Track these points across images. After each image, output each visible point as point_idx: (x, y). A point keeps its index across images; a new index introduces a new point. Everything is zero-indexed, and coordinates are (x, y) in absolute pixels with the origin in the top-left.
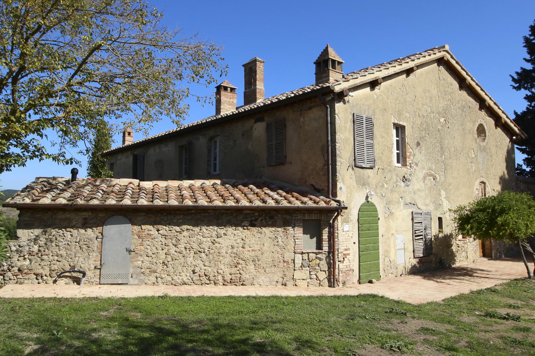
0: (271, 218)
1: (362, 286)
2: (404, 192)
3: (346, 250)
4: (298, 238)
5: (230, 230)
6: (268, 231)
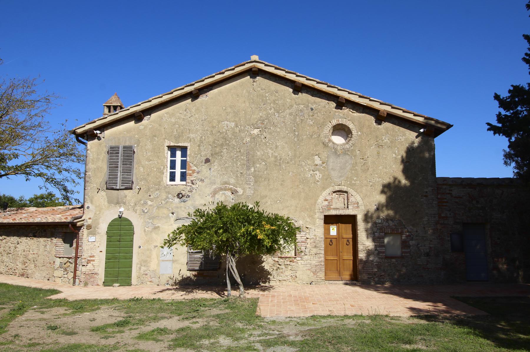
0: (45, 231)
1: (76, 288)
2: (177, 208)
3: (91, 257)
4: (56, 246)
5: (24, 240)
6: (42, 240)
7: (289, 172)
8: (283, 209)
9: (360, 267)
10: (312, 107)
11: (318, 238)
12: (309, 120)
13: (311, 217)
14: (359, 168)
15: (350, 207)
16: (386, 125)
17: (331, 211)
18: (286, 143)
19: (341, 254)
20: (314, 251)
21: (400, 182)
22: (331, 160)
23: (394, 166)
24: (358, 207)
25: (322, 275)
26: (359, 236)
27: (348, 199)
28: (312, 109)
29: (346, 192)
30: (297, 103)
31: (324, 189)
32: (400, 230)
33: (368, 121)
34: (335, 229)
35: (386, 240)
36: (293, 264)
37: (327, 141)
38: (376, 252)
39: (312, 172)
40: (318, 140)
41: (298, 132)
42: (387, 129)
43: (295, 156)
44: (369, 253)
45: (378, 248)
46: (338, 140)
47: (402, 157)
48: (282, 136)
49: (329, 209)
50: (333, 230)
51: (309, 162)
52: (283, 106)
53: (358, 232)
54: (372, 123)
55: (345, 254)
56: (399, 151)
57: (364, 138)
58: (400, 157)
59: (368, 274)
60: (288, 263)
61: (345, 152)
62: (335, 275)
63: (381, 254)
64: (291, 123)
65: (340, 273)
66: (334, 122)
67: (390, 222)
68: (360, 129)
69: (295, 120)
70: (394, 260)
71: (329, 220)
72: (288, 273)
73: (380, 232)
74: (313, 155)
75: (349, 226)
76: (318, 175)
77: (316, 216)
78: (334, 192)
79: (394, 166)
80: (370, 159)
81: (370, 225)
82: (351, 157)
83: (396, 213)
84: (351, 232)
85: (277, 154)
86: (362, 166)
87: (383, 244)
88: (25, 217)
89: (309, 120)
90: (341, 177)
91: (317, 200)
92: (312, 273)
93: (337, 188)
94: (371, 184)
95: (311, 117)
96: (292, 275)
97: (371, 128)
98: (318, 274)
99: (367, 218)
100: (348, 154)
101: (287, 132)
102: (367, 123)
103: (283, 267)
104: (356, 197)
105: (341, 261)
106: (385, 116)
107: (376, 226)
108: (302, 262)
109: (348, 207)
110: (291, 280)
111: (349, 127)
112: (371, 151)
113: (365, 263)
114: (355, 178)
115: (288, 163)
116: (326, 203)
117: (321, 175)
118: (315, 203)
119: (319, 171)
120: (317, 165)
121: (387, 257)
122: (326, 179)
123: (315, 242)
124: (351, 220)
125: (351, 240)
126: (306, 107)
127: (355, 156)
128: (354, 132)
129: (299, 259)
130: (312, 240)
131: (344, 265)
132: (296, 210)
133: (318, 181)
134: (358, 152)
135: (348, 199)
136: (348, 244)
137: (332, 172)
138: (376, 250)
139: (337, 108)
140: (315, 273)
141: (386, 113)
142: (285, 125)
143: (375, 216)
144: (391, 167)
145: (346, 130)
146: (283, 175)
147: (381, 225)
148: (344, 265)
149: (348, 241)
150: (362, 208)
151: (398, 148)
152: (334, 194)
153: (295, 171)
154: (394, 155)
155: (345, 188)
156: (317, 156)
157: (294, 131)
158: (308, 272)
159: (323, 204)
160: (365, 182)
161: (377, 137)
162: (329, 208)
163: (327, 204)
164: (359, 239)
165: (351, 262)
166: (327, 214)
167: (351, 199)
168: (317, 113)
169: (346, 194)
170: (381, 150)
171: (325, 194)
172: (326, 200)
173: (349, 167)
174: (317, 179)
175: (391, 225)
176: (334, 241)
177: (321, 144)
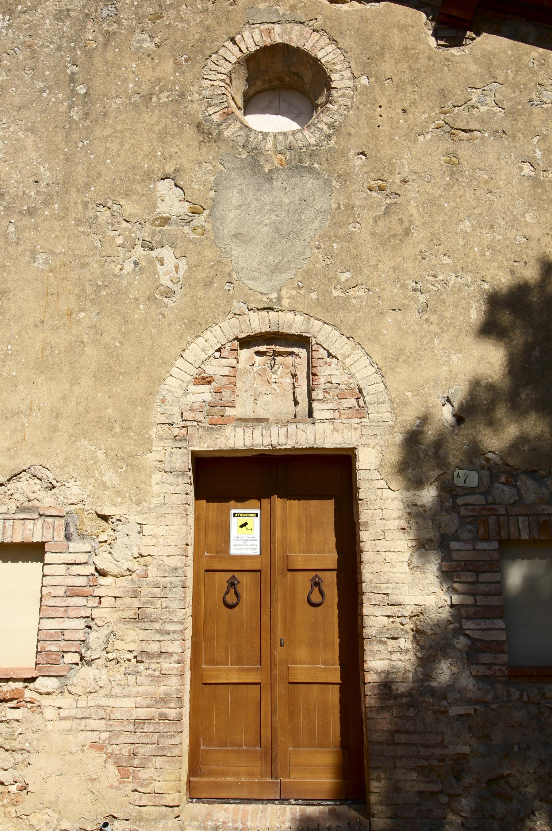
7: (34, 255)
9: (380, 724)
11: (153, 572)
12: (138, 36)
14: (363, 230)
17: (229, 430)
18: (32, 130)
19: (280, 653)
20: (132, 639)
22: (233, 197)
23: (529, 218)
24: (361, 410)
25: (170, 775)
26: (366, 556)
27: (311, 375)
29: (303, 341)
31: (196, 326)
33: (402, 28)
34: (255, 523)
37: (216, 118)
38: (461, 642)
39: (139, 252)
40: (175, 114)
41: (87, 82)
42: (487, 61)
43: (67, 182)
44: (432, 642)
45: (468, 625)
48: (17, 100)
49: (216, 425)
50: (245, 533)
51: (129, 208)
53: (364, 535)
54: (418, 39)
55: (302, 653)
57: (383, 101)
59: (420, 770)
61: (299, 161)
62: (246, 771)
63: (486, 658)
64: (59, 48)
65: (272, 760)
67: (527, 485)
68: (368, 63)
69: (76, 38)
71: (220, 478)
73: (476, 539)
74: (149, 177)
75: (325, 509)
77: (152, 458)
78: (246, 342)
79: (529, 218)
80: (413, 190)
81: (429, 495)
82: (328, 183)
84: (332, 541)
87: (495, 601)
88: (267, 219)
89: (138, 36)
90: (277, 269)
92: (112, 771)
93: (258, 323)
94: (422, 298)
97: (416, 59)
98: (144, 774)
99: (418, 454)
102: (396, 39)
104: (348, 363)
105: (281, 689)
107: (455, 507)
108: (64, 701)
109: (310, 414)
111: (316, 60)
112: (419, 156)
113: (411, 699)
114: (345, 276)
115: (31, 212)
116: (204, 393)
117: (183, 264)
118: (151, 393)
119: (173, 245)
120: (166, 221)
121: (518, 674)
122: (208, 284)
123: (135, 595)
124: (326, 475)
125: (330, 581)
127: (343, 178)
128: (340, 79)
129: (51, 684)
131: (293, 713)
132: (55, 430)
133: (169, 293)
134: (359, 161)
135: (311, 375)
136: (316, 598)
137: (238, 254)
140: (126, 767)
142: (34, 55)
144: (514, 219)
147: (478, 499)
148: (293, 713)
149: (316, 584)
150: (381, 413)
152: (246, 354)
153: (59, 249)
154: (527, 169)
155: (294, 324)
157: (72, 78)
158: (94, 762)
159: (190, 398)
160: (392, 292)
161: (443, 94)
162: (216, 415)
163: (208, 397)
164: (368, 573)
165: (334, 696)
167: (327, 372)
169: (303, 352)
172: (206, 380)
173: (314, 226)
174: (166, 281)
175: (530, 498)
176: (245, 579)
177: (190, 132)
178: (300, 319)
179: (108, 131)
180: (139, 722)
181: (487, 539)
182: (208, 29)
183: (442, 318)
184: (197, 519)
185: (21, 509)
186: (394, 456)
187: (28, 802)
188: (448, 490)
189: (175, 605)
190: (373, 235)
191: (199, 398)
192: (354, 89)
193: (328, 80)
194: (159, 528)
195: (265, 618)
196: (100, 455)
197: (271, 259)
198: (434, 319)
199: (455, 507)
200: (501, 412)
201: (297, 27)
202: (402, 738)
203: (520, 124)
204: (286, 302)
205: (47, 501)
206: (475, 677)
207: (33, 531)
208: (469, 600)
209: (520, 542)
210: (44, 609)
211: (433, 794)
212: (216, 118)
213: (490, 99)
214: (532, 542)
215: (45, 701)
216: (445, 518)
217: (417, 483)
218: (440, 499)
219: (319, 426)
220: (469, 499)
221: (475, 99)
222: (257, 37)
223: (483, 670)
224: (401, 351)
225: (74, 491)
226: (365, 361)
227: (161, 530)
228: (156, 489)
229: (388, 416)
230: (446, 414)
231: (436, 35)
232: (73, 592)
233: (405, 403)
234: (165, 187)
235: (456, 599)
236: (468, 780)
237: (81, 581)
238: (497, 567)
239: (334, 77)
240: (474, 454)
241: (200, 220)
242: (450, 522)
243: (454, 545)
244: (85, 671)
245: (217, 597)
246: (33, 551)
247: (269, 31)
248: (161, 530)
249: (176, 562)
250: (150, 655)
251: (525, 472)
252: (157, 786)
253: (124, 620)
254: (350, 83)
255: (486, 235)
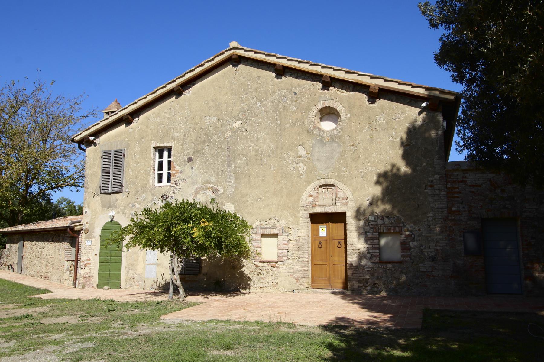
7: (271, 167)
8: (264, 208)
10: (296, 91)
11: (301, 240)
12: (292, 106)
13: (294, 215)
15: (338, 203)
16: (382, 103)
17: (317, 208)
18: (268, 134)
19: (331, 258)
20: (297, 254)
21: (398, 169)
22: (317, 150)
23: (390, 152)
24: (347, 203)
25: (307, 281)
28: (295, 93)
29: (334, 186)
30: (280, 89)
31: (308, 183)
32: (397, 230)
33: (359, 99)
34: (325, 229)
35: (383, 241)
36: (275, 269)
37: (312, 128)
38: (369, 255)
39: (295, 165)
41: (280, 120)
44: (361, 256)
45: (370, 251)
46: (328, 126)
47: (401, 139)
48: (264, 127)
49: (314, 206)
50: (323, 231)
52: (266, 93)
54: (364, 103)
56: (396, 133)
57: (354, 121)
58: (398, 139)
59: (359, 282)
60: (270, 268)
61: (333, 138)
63: (374, 258)
64: (273, 111)
65: (329, 280)
66: (320, 106)
67: (386, 220)
68: (350, 110)
70: (390, 266)
71: (317, 219)
72: (269, 279)
73: (373, 232)
74: (296, 145)
75: (343, 224)
76: (302, 168)
77: (300, 215)
78: (320, 186)
79: (390, 152)
80: (361, 145)
81: (362, 223)
83: (394, 207)
85: (258, 148)
86: (352, 154)
89: (292, 106)
90: (327, 168)
91: (301, 196)
92: (294, 280)
93: (323, 182)
94: (362, 174)
95: (294, 103)
96: (273, 281)
98: (301, 281)
99: (359, 214)
100: (335, 141)
101: (269, 122)
103: (264, 272)
104: (345, 191)
106: (377, 91)
108: (283, 266)
110: (272, 287)
111: (337, 110)
113: (357, 268)
114: (344, 169)
115: (269, 156)
116: (311, 199)
117: (305, 168)
118: (299, 200)
119: (303, 163)
120: (300, 157)
122: (311, 172)
123: (297, 245)
124: (338, 218)
126: (289, 92)
129: (281, 263)
130: (295, 242)
132: (278, 208)
133: (302, 175)
134: (347, 138)
138: (368, 253)
139: (323, 89)
140: (297, 279)
141: (377, 89)
143: (368, 212)
144: (387, 152)
145: (336, 113)
146: (264, 170)
147: (374, 223)
151: (396, 129)
152: (321, 189)
153: (277, 165)
154: (391, 138)
155: (332, 182)
156: (301, 146)
157: (277, 120)
158: (291, 278)
159: (308, 201)
161: (370, 118)
166: (311, 212)
167: (340, 194)
168: (301, 97)
169: (334, 188)
170: (374, 134)
171: (310, 188)
172: (311, 196)
174: (301, 172)
175: (386, 223)
177: (305, 132)
178: (333, 180)
179: (286, 134)
180: (300, 271)
181: (376, 232)
182: (309, 103)
183: (367, 179)
184: (311, 228)
185: (272, 226)
186: (354, 214)
187: (278, 286)
188: (367, 222)
189: (306, 247)
190: (351, 158)
191: (310, 200)
192: (346, 118)
193: (340, 116)
194: (303, 230)
195: (328, 251)
196: (288, 214)
197: (326, 166)
198: (365, 179)
199: (369, 225)
200: (379, 203)
201: (332, 101)
202: (355, 275)
203: (389, 126)
204: (329, 176)
205: (278, 224)
206: (372, 263)
207: (275, 231)
208: (371, 246)
209: (383, 233)
210: (279, 248)
211: (361, 286)
212: (312, 128)
213: (382, 119)
214: (386, 233)
215: (280, 266)
216: (366, 228)
217: (359, 220)
218: (365, 223)
219: (337, 207)
220: (372, 223)
221: (378, 119)
222: (322, 104)
223: (373, 261)
224: (357, 188)
225: (283, 222)
226: (349, 190)
227: (302, 231)
228: (301, 222)
229: (354, 204)
230: (367, 203)
231: (368, 101)
232: (284, 244)
233: (358, 201)
234: (300, 148)
235: (368, 246)
236: (369, 284)
237: (286, 242)
238: (379, 239)
239: (341, 115)
240: (372, 214)
241: (309, 156)
242: (367, 229)
243: (368, 234)
244: (288, 261)
245: (317, 246)
246: (275, 235)
247: (325, 103)
248: (302, 231)
249: (306, 238)
250: (301, 257)
251: (386, 217)
252: (304, 283)
253: (296, 250)
254: (345, 116)
255: (379, 157)
